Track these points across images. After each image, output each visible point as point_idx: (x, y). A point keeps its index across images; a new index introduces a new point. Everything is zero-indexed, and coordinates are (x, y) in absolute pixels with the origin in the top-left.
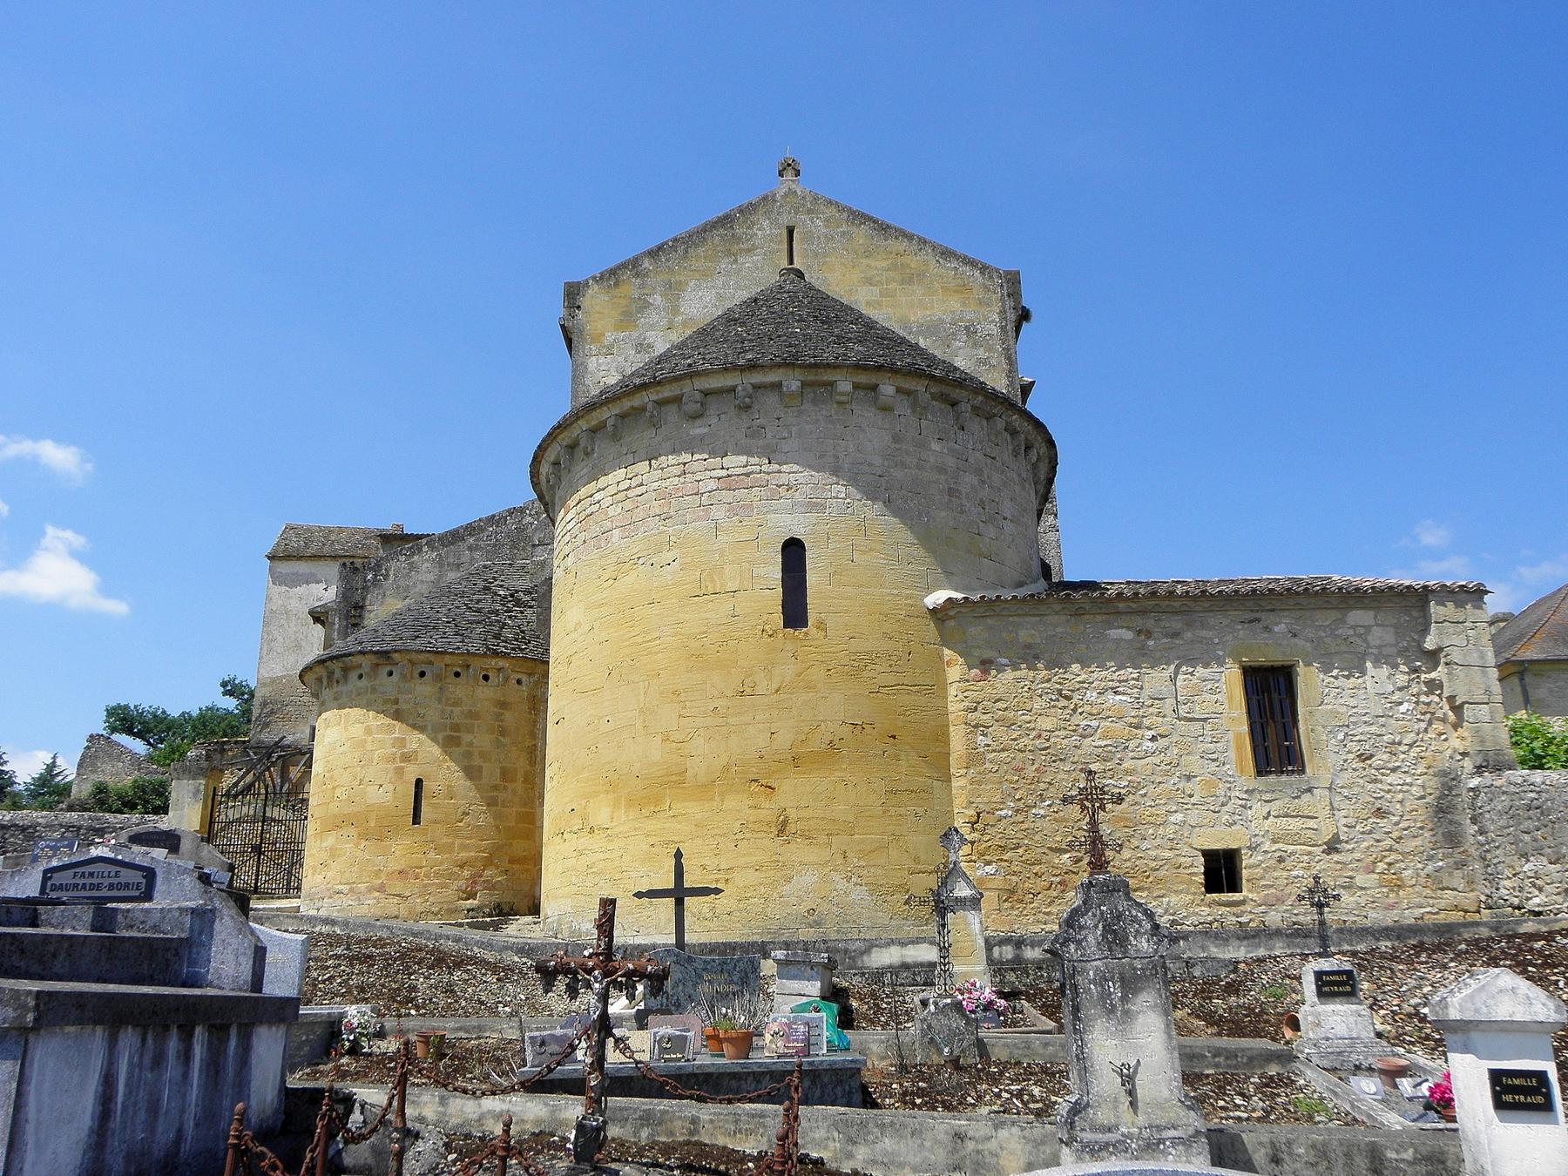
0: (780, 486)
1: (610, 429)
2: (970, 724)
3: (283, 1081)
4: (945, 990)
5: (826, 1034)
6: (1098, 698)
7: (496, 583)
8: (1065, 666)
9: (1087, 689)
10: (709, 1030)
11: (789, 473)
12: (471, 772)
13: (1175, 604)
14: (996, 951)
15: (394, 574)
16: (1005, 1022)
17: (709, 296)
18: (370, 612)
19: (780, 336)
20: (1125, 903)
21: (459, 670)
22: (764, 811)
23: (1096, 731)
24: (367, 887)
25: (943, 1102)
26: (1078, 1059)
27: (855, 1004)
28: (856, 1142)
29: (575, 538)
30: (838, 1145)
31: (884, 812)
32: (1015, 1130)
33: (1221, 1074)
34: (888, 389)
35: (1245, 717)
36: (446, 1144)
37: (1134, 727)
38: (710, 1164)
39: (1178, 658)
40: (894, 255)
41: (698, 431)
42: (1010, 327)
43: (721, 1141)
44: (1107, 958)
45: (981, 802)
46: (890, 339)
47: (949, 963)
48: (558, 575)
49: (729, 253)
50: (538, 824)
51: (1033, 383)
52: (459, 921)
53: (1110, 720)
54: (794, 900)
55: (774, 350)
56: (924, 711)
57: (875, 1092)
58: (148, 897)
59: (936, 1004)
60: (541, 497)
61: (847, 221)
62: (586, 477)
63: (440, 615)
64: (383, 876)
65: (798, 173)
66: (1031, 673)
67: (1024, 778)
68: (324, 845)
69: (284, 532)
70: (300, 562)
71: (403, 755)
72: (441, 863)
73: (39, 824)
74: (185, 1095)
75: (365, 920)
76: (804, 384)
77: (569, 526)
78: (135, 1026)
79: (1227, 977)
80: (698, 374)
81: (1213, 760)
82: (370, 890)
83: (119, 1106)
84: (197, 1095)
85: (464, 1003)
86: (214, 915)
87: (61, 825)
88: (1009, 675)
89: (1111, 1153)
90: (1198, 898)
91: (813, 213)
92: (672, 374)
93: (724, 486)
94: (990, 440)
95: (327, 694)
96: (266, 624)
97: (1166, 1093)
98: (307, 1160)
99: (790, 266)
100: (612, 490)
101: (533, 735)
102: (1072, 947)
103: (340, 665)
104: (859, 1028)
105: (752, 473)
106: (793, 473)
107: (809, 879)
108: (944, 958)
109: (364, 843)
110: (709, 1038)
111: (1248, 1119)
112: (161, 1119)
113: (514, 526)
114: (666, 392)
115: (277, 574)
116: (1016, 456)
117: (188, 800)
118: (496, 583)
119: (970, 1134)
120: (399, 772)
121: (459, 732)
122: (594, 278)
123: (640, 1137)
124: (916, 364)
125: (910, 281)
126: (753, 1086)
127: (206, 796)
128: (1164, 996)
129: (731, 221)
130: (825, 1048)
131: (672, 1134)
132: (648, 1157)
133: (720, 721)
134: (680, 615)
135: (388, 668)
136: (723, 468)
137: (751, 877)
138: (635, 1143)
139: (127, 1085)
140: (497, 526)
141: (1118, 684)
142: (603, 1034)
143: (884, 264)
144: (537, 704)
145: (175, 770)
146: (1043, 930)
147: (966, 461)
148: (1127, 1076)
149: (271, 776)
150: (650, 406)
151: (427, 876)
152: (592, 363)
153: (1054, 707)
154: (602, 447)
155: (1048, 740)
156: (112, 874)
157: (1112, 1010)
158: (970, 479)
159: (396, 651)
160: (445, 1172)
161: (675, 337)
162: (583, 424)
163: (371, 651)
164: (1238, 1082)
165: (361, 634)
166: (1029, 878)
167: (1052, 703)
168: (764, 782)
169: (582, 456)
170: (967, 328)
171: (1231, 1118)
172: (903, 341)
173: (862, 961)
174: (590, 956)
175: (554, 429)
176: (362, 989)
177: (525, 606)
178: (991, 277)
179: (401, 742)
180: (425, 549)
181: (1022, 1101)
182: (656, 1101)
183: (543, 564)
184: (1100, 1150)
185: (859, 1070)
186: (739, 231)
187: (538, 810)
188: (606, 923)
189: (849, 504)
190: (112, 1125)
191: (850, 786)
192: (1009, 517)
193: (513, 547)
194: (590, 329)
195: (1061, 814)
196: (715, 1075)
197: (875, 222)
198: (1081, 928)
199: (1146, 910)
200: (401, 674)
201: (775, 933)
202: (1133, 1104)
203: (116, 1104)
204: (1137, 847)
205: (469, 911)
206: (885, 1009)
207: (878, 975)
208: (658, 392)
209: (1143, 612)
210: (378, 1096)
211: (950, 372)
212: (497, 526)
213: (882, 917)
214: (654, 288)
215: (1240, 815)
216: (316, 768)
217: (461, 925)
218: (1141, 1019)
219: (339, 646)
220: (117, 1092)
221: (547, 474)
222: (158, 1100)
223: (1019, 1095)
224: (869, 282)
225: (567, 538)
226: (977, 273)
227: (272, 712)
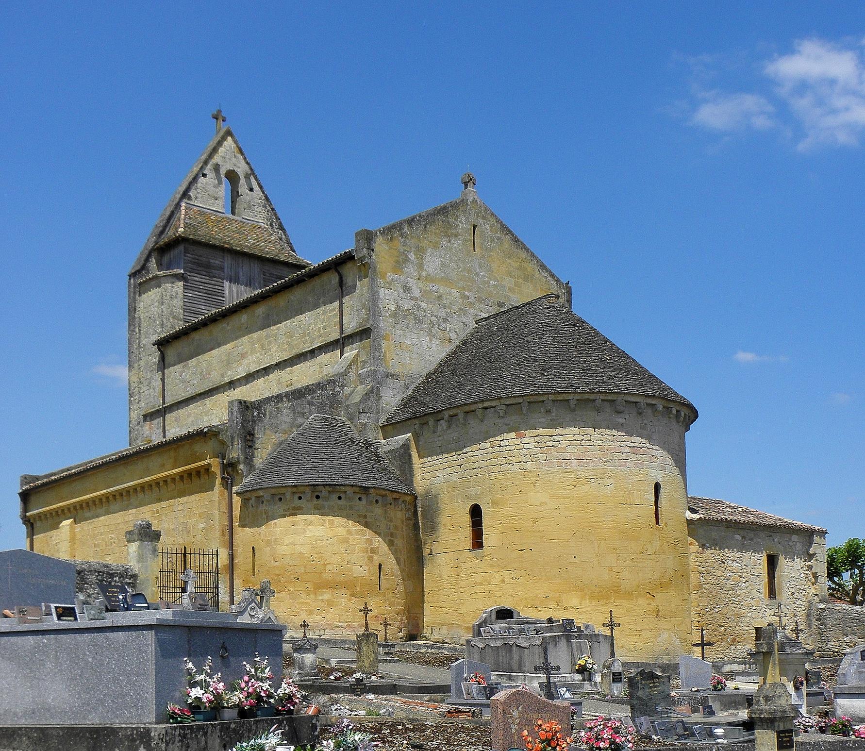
0: (653, 456)
18: (258, 438)
24: (359, 624)
49: (447, 236)
68: (320, 598)
71: (372, 549)
87: (95, 571)
88: (709, 551)
100: (570, 437)
105: (643, 447)
109: (354, 600)
120: (370, 559)
129: (447, 212)
134: (616, 512)
168: (651, 593)
179: (369, 541)
193: (331, 407)
197: (513, 235)
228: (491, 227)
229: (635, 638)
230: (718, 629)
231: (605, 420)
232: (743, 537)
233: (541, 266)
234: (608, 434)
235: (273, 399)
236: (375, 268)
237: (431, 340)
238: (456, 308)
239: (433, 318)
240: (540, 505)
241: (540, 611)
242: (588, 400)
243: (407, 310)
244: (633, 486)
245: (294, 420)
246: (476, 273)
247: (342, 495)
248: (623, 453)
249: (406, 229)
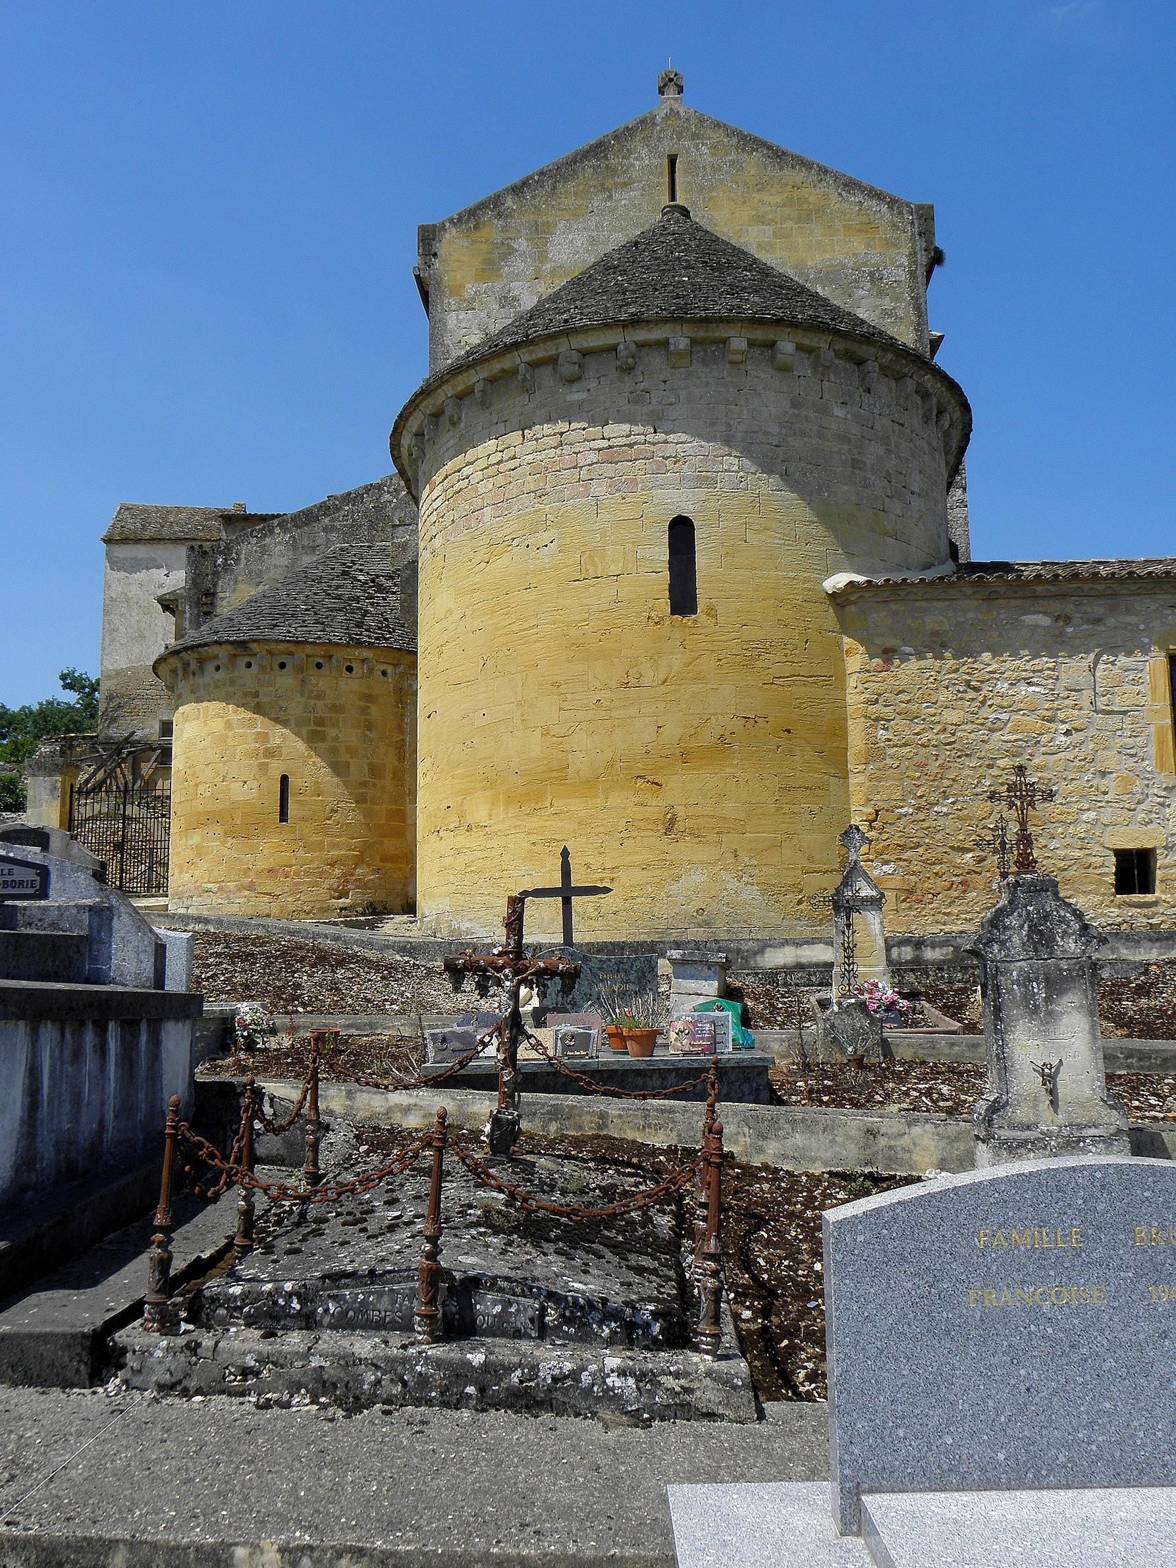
1: (478, 395)
2: (870, 718)
3: (192, 1075)
4: (849, 990)
5: (731, 1033)
6: (1009, 689)
7: (355, 567)
8: (974, 654)
9: (997, 679)
10: (612, 1029)
11: (677, 443)
12: (338, 768)
13: (1098, 587)
14: (895, 952)
15: (246, 558)
16: (906, 1022)
17: (581, 240)
18: (222, 599)
19: (665, 286)
20: (1053, 903)
21: (321, 661)
22: (651, 809)
23: (1006, 725)
25: (851, 1099)
26: (999, 1059)
27: (750, 1004)
28: (766, 1138)
29: (442, 517)
30: (748, 1140)
31: (778, 810)
32: (928, 1127)
33: (1133, 1075)
34: (787, 346)
35: (1168, 710)
36: (356, 1136)
37: (1048, 721)
38: (623, 1157)
39: (1099, 646)
40: (789, 188)
41: (576, 397)
42: (921, 272)
43: (630, 1135)
44: (1031, 958)
45: (880, 799)
46: (789, 288)
47: (853, 963)
48: (424, 558)
49: (603, 188)
50: (409, 822)
51: (941, 337)
52: (333, 919)
53: (1022, 712)
54: (683, 900)
55: (660, 302)
56: (821, 704)
57: (780, 1089)
58: (43, 894)
59: (839, 1004)
60: (402, 473)
61: (737, 148)
62: (453, 449)
63: (298, 603)
64: (252, 874)
65: (680, 90)
66: (938, 663)
67: (926, 775)
68: (190, 842)
69: (119, 513)
70: (138, 546)
72: (311, 862)
74: (103, 1088)
75: (239, 919)
76: (694, 342)
77: (435, 505)
78: (53, 1021)
79: (1137, 979)
80: (575, 331)
81: (1132, 756)
82: (240, 888)
83: (45, 1098)
84: (115, 1089)
85: (350, 1001)
86: (111, 912)
88: (913, 665)
89: (1030, 1150)
90: (1108, 899)
91: (698, 139)
92: (546, 332)
93: (605, 458)
94: (898, 404)
95: (183, 686)
96: (106, 612)
97: (1088, 1092)
98: (235, 1150)
99: (672, 203)
100: (482, 463)
101: (401, 729)
102: (996, 947)
103: (196, 655)
104: (756, 1027)
105: (635, 444)
106: (681, 443)
107: (697, 878)
108: (848, 958)
109: (230, 841)
110: (611, 1035)
111: (1163, 1119)
112: (84, 1110)
113: (372, 505)
114: (540, 352)
115: (115, 559)
116: (926, 423)
118: (355, 567)
119: (883, 1130)
120: (263, 767)
121: (323, 726)
122: (451, 220)
123: (548, 1131)
124: (819, 317)
125: (808, 219)
126: (659, 1082)
127: (63, 793)
128: (1090, 997)
129: (605, 149)
130: (731, 1046)
131: (580, 1128)
132: (560, 1150)
135: (246, 660)
136: (603, 438)
137: (638, 876)
138: (544, 1136)
139: (51, 1078)
140: (353, 505)
141: (1031, 675)
142: (514, 1031)
143: (779, 199)
144: (406, 697)
145: (30, 766)
146: (941, 930)
147: (872, 428)
148: (1048, 1076)
149: (122, 772)
150: (522, 368)
151: (297, 874)
152: (451, 319)
153: (961, 699)
154: (470, 416)
155: (953, 734)
156: (6, 872)
157: (1035, 1011)
158: (876, 449)
159: (255, 641)
160: (360, 1162)
161: (545, 289)
162: (448, 390)
163: (228, 642)
164: (1152, 1083)
165: (215, 623)
166: (929, 878)
167: (960, 695)
168: (650, 778)
169: (448, 426)
170: (871, 274)
171: (1147, 1118)
172: (803, 291)
173: (755, 961)
174: (500, 954)
175: (417, 395)
176: (246, 987)
177: (387, 592)
178: (900, 213)
179: (264, 737)
180: (277, 530)
181: (932, 1100)
182: (561, 1096)
183: (404, 546)
184: (1018, 1147)
185: (766, 1068)
186: (613, 161)
187: (409, 807)
188: (515, 923)
189: (742, 477)
190: (40, 1115)
191: (742, 784)
192: (917, 490)
193: (372, 527)
194: (448, 281)
195: (965, 812)
196: (620, 1073)
197: (769, 148)
198: (1006, 928)
199: (1075, 911)
200: (260, 665)
201: (662, 933)
202: (1054, 1103)
203: (42, 1095)
204: (1045, 846)
205: (341, 909)
206: (781, 1008)
207: (772, 976)
208: (531, 352)
209: (1063, 596)
210: (284, 1090)
211: (857, 326)
212: (353, 505)
213: (775, 918)
214: (519, 231)
215: (1157, 814)
216: (177, 764)
217: (335, 924)
218: (1065, 1019)
219: (193, 636)
220: (42, 1083)
221: (409, 446)
222: (80, 1092)
223: (928, 1093)
224: (761, 220)
225: (433, 518)
226: (885, 208)
227: (119, 706)
230: (946, 858)
232: (1058, 618)
233: (845, 185)
244: (603, 536)
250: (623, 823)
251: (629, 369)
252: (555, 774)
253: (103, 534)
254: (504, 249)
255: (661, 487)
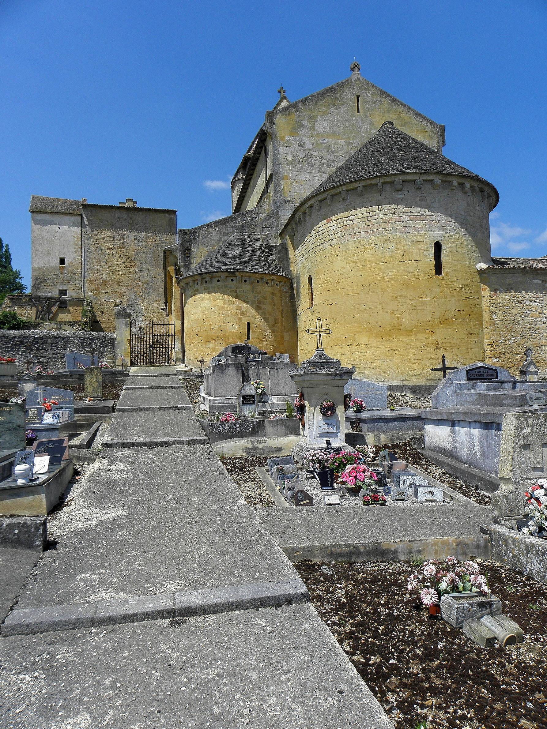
8: (520, 292)
12: (266, 320)
40: (398, 113)
68: (208, 346)
71: (241, 312)
73: (69, 337)
88: (503, 294)
96: (33, 243)
100: (360, 216)
105: (422, 215)
117: (123, 327)
120: (240, 319)
121: (261, 304)
133: (414, 308)
135: (231, 278)
140: (242, 218)
152: (281, 149)
159: (237, 272)
178: (434, 127)
179: (240, 308)
193: (249, 227)
197: (391, 97)
208: (384, 179)
227: (41, 283)
228: (372, 94)
229: (414, 366)
231: (386, 198)
232: (543, 281)
233: (416, 115)
234: (389, 208)
235: (205, 226)
236: (276, 135)
237: (321, 175)
238: (342, 152)
239: (323, 161)
240: (341, 270)
241: (342, 348)
242: (371, 185)
243: (301, 158)
244: (412, 246)
245: (221, 238)
246: (360, 127)
247: (234, 279)
248: (403, 222)
249: (300, 106)
250: (422, 344)
251: (419, 189)
252: (396, 327)
253: (29, 209)
254: (299, 124)
255: (431, 231)
